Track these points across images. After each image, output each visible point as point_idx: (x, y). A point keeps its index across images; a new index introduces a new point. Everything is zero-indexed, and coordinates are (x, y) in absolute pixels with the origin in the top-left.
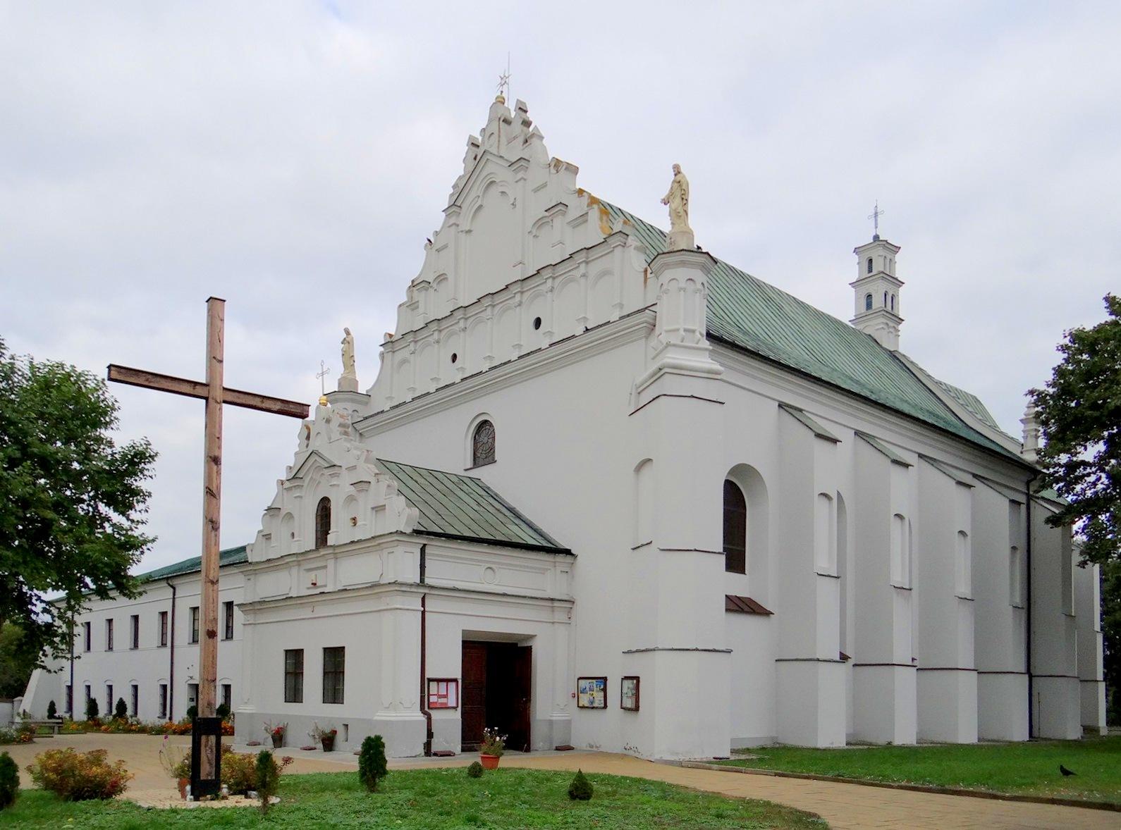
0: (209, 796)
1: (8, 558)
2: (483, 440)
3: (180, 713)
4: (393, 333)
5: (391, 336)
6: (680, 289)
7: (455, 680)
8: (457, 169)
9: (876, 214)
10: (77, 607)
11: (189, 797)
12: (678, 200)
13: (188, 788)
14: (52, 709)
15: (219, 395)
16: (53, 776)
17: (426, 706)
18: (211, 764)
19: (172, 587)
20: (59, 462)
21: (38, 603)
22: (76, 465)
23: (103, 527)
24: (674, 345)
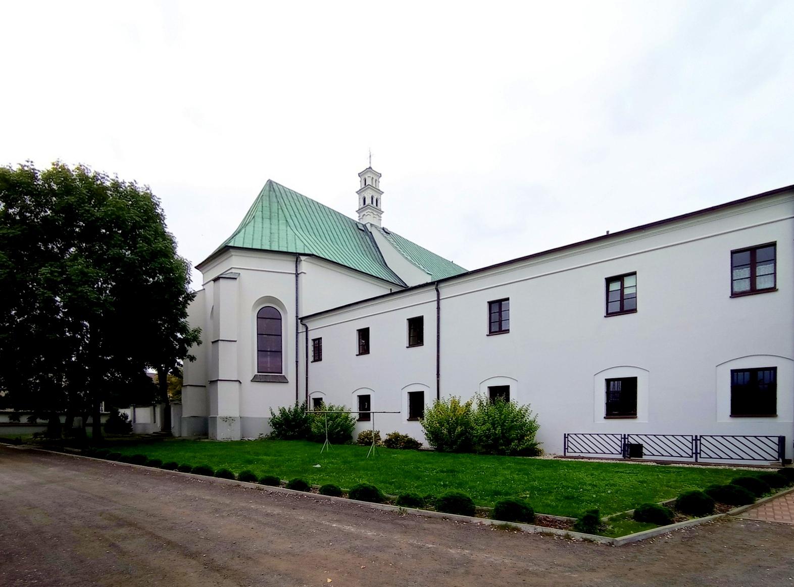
9: (370, 156)
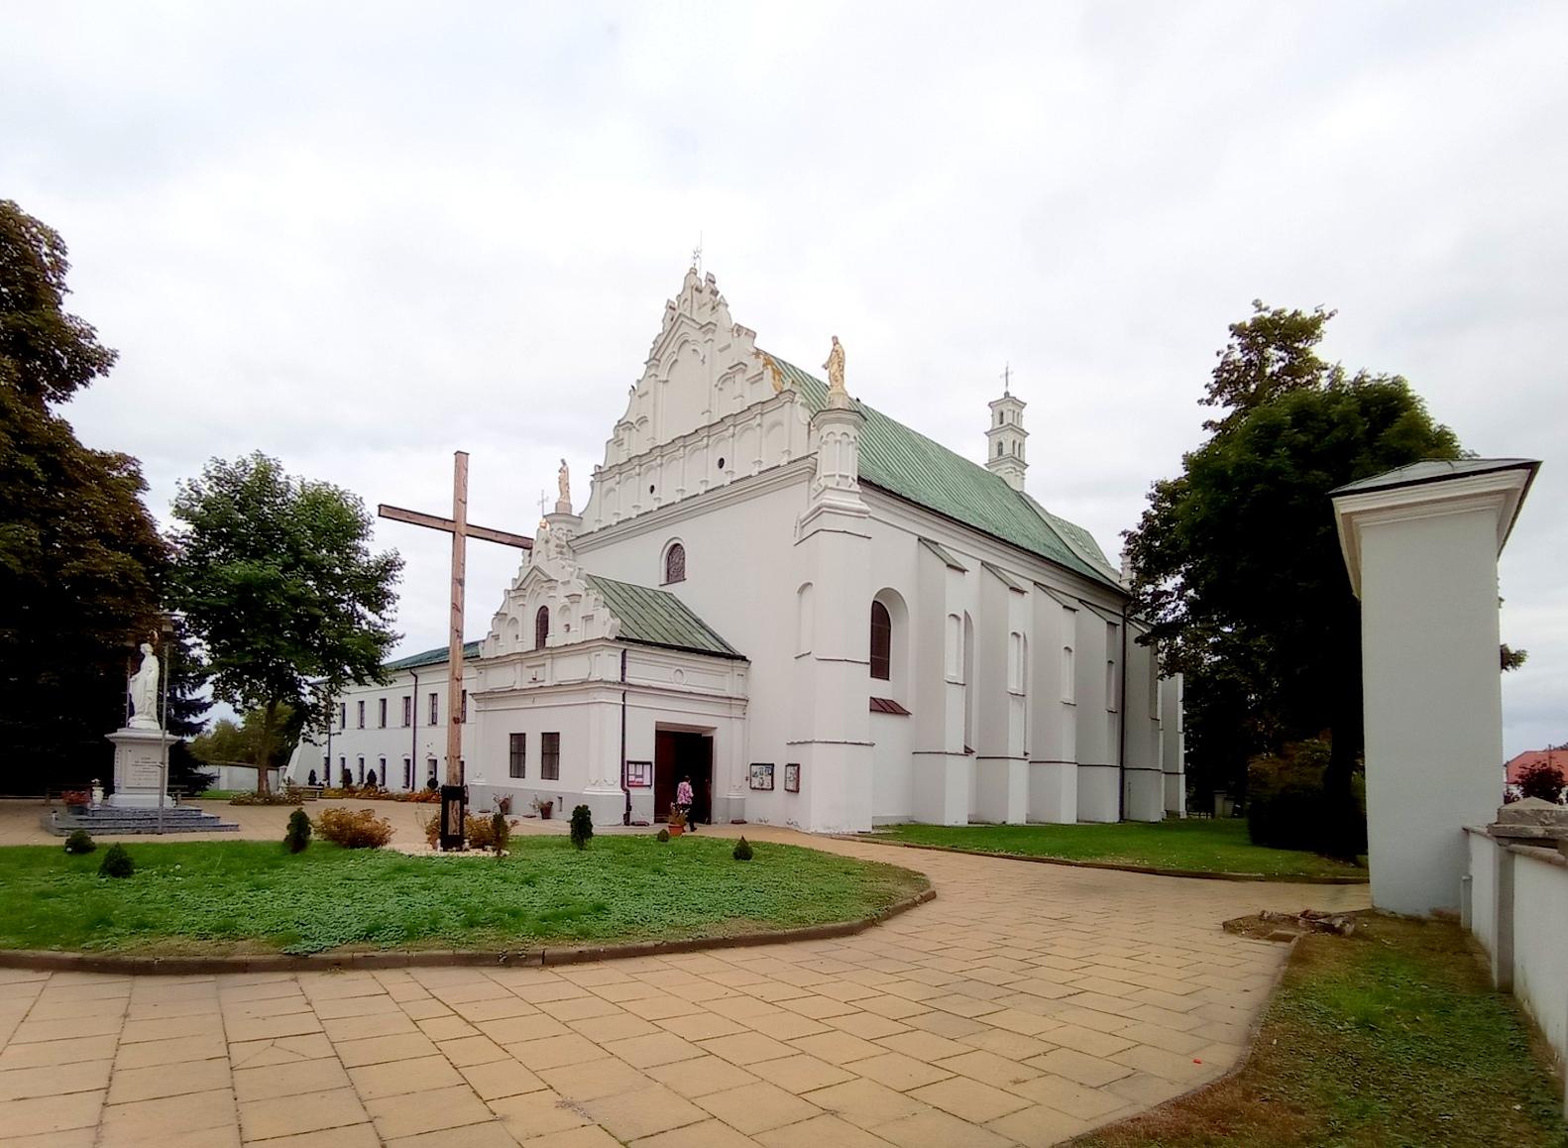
0: (454, 849)
1: (283, 647)
2: (675, 568)
3: (421, 784)
4: (602, 464)
5: (600, 467)
6: (836, 442)
7: (650, 763)
8: (657, 328)
9: (1007, 374)
10: (338, 691)
11: (440, 848)
12: (836, 366)
13: (439, 841)
14: (312, 777)
15: (463, 530)
16: (334, 828)
17: (626, 784)
18: (456, 822)
19: (415, 675)
20: (324, 567)
21: (306, 686)
22: (338, 570)
23: (359, 623)
24: (831, 488)
